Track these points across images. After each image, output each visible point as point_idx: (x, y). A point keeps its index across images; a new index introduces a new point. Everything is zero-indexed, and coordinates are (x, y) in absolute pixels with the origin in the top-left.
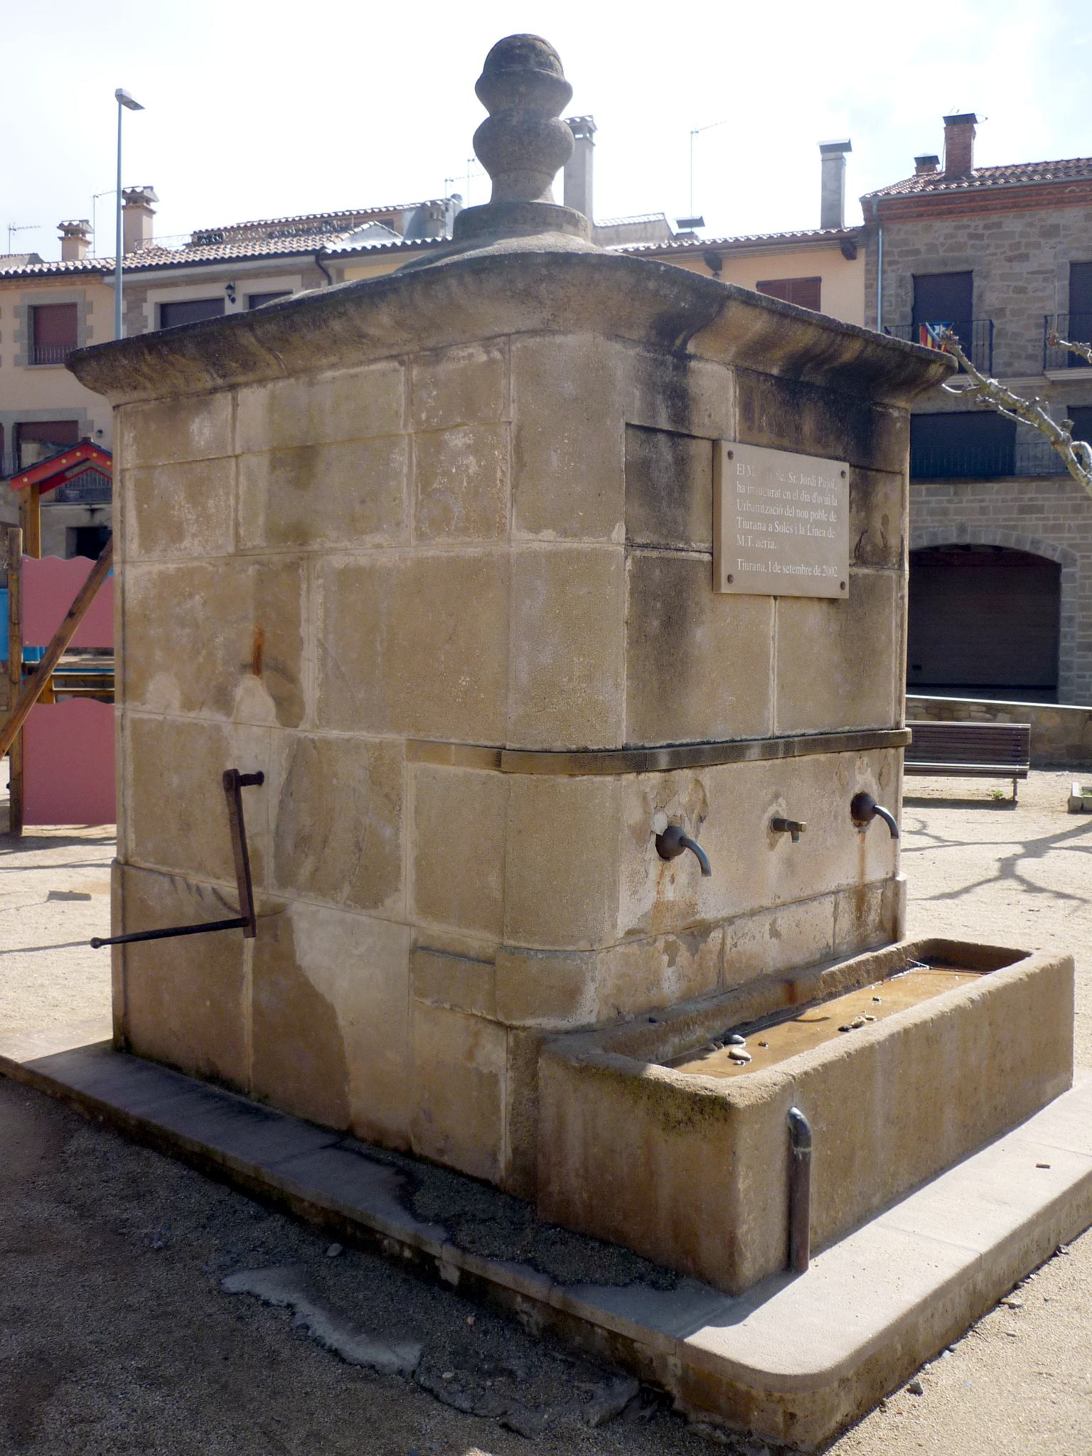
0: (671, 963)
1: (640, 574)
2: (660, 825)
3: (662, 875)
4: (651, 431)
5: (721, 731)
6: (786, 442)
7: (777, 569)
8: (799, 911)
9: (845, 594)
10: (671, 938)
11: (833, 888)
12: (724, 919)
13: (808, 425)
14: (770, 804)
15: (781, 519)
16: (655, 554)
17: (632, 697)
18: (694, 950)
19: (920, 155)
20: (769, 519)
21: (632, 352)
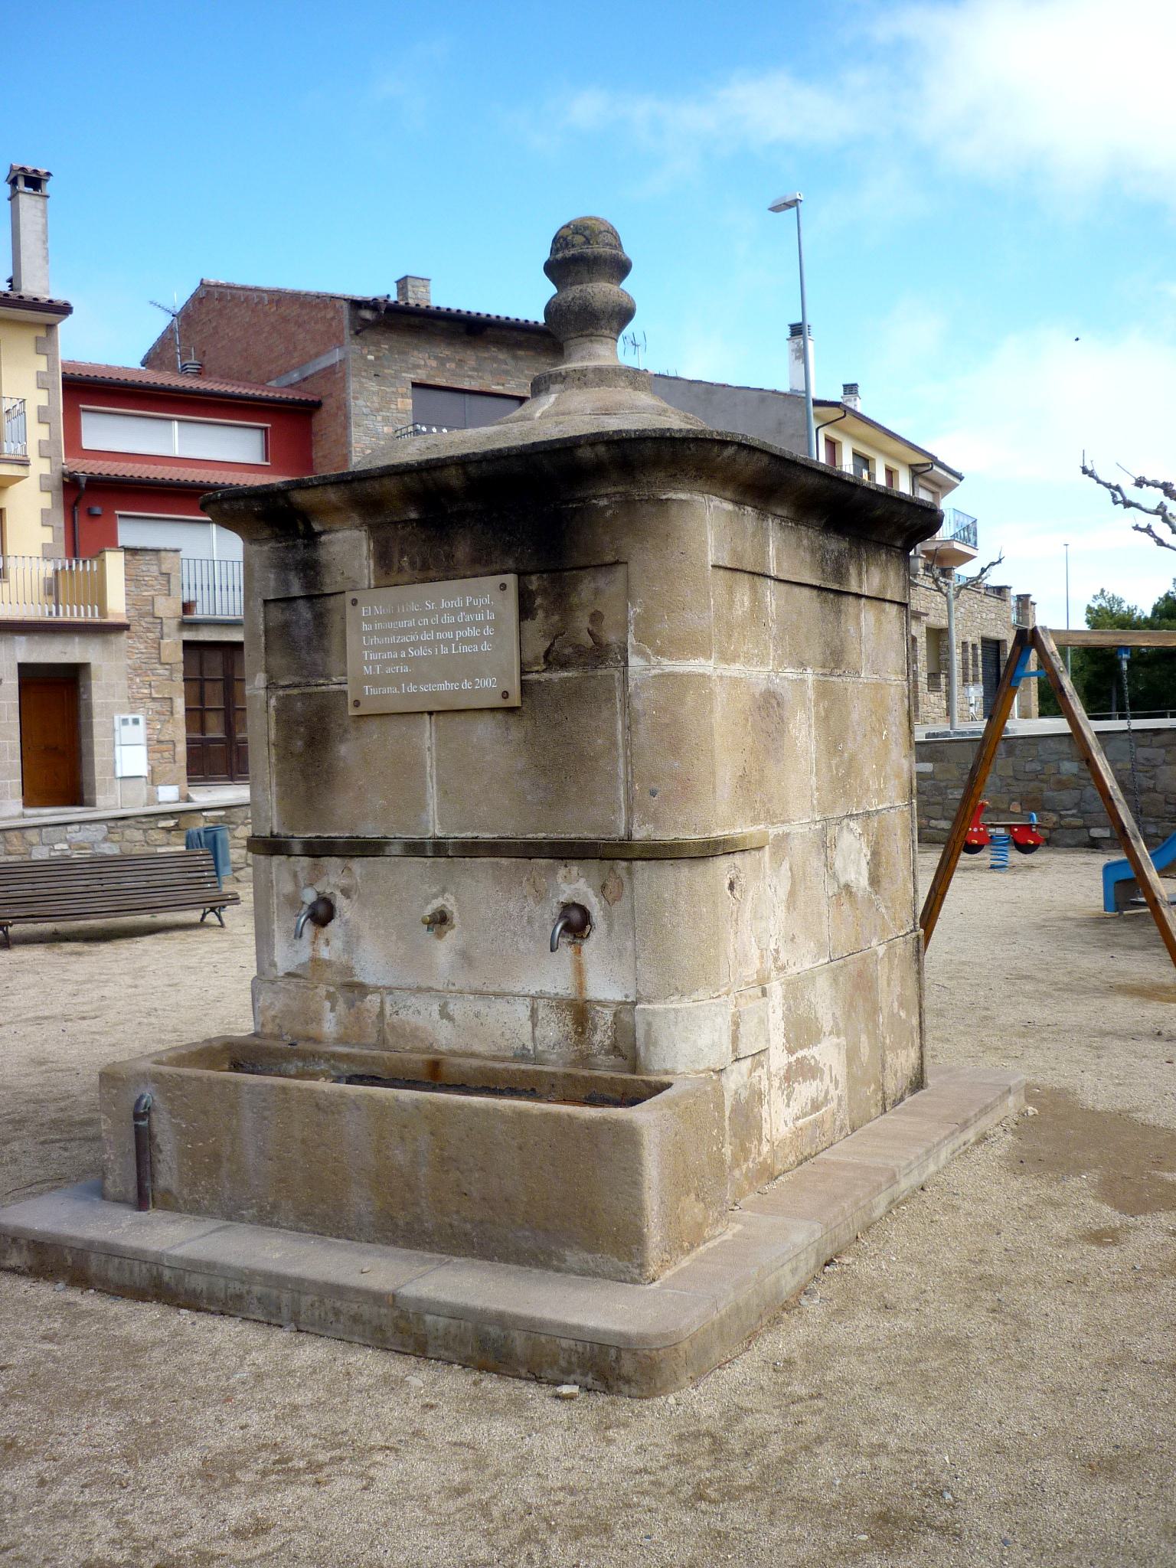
0: (332, 1010)
1: (284, 708)
2: (309, 896)
3: (316, 936)
4: (290, 600)
5: (370, 830)
6: (432, 574)
7: (412, 689)
8: (480, 1006)
9: (515, 700)
10: (332, 989)
11: (532, 992)
12: (385, 988)
13: (462, 550)
14: (435, 896)
15: (415, 645)
16: (295, 691)
17: (281, 798)
18: (351, 1005)
19: (397, 278)
20: (403, 646)
21: (266, 548)
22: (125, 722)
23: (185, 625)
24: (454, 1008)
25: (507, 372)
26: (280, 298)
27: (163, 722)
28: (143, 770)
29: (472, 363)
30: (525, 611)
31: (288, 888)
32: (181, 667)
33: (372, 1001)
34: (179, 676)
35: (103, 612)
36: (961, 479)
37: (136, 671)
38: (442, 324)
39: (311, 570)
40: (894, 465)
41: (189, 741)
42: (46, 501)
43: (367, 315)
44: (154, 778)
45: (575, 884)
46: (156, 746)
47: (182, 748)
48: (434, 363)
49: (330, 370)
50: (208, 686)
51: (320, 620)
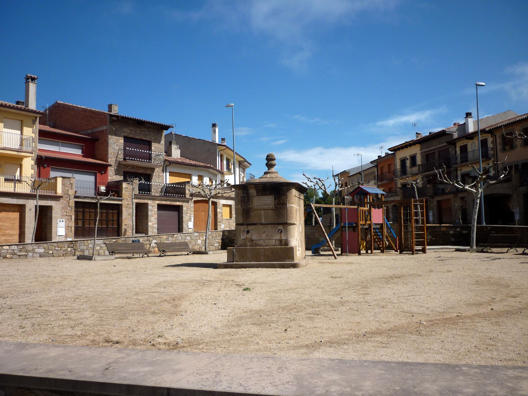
2: (246, 230)
5: (255, 222)
22: (60, 221)
23: (76, 197)
24: (266, 241)
25: (147, 134)
26: (85, 110)
27: (69, 222)
28: (64, 234)
29: (138, 132)
30: (275, 199)
31: (243, 229)
32: (74, 208)
33: (255, 241)
34: (73, 210)
35: (56, 193)
36: (251, 165)
37: (63, 208)
38: (131, 121)
39: (248, 194)
40: (229, 157)
41: (75, 227)
42: (33, 162)
43: (115, 118)
44: (66, 236)
45: (280, 227)
46: (67, 228)
47: (73, 229)
48: (129, 131)
49: (103, 131)
50: (91, 213)
51: (249, 199)
